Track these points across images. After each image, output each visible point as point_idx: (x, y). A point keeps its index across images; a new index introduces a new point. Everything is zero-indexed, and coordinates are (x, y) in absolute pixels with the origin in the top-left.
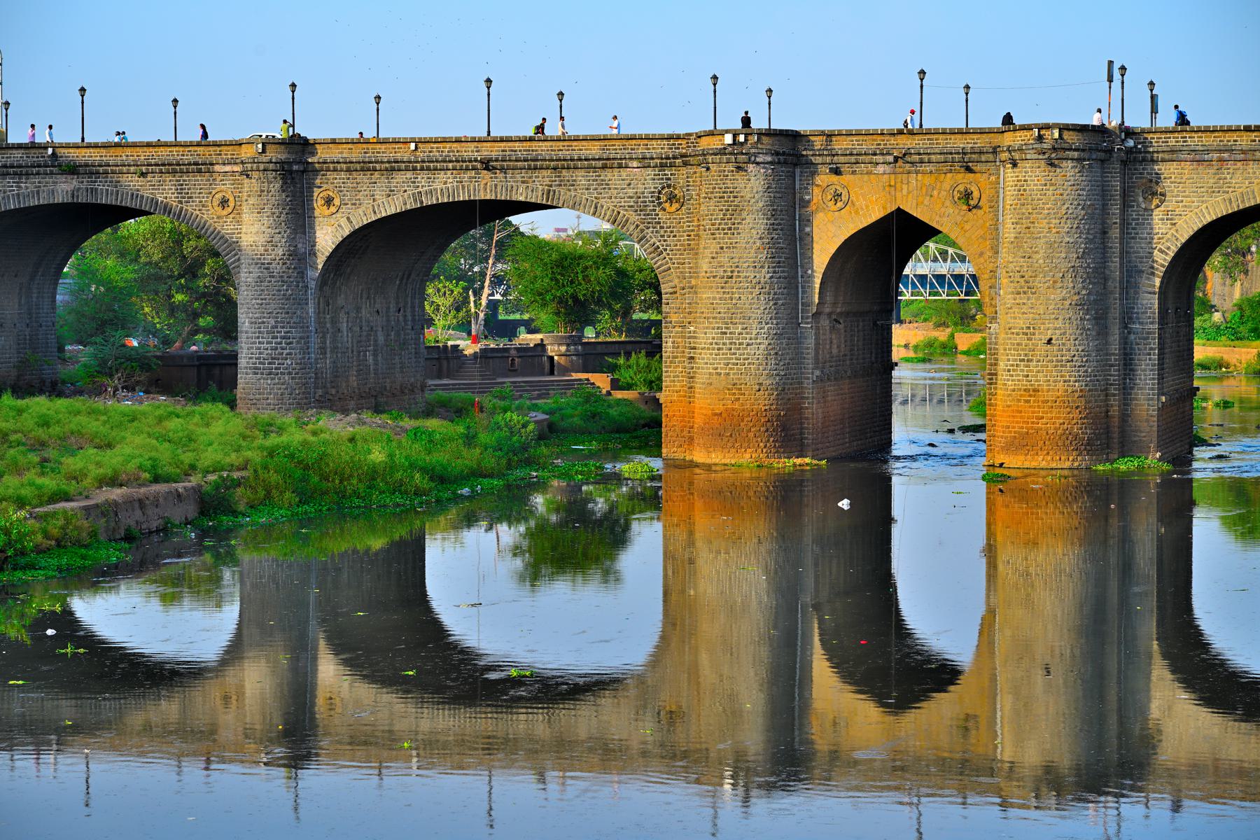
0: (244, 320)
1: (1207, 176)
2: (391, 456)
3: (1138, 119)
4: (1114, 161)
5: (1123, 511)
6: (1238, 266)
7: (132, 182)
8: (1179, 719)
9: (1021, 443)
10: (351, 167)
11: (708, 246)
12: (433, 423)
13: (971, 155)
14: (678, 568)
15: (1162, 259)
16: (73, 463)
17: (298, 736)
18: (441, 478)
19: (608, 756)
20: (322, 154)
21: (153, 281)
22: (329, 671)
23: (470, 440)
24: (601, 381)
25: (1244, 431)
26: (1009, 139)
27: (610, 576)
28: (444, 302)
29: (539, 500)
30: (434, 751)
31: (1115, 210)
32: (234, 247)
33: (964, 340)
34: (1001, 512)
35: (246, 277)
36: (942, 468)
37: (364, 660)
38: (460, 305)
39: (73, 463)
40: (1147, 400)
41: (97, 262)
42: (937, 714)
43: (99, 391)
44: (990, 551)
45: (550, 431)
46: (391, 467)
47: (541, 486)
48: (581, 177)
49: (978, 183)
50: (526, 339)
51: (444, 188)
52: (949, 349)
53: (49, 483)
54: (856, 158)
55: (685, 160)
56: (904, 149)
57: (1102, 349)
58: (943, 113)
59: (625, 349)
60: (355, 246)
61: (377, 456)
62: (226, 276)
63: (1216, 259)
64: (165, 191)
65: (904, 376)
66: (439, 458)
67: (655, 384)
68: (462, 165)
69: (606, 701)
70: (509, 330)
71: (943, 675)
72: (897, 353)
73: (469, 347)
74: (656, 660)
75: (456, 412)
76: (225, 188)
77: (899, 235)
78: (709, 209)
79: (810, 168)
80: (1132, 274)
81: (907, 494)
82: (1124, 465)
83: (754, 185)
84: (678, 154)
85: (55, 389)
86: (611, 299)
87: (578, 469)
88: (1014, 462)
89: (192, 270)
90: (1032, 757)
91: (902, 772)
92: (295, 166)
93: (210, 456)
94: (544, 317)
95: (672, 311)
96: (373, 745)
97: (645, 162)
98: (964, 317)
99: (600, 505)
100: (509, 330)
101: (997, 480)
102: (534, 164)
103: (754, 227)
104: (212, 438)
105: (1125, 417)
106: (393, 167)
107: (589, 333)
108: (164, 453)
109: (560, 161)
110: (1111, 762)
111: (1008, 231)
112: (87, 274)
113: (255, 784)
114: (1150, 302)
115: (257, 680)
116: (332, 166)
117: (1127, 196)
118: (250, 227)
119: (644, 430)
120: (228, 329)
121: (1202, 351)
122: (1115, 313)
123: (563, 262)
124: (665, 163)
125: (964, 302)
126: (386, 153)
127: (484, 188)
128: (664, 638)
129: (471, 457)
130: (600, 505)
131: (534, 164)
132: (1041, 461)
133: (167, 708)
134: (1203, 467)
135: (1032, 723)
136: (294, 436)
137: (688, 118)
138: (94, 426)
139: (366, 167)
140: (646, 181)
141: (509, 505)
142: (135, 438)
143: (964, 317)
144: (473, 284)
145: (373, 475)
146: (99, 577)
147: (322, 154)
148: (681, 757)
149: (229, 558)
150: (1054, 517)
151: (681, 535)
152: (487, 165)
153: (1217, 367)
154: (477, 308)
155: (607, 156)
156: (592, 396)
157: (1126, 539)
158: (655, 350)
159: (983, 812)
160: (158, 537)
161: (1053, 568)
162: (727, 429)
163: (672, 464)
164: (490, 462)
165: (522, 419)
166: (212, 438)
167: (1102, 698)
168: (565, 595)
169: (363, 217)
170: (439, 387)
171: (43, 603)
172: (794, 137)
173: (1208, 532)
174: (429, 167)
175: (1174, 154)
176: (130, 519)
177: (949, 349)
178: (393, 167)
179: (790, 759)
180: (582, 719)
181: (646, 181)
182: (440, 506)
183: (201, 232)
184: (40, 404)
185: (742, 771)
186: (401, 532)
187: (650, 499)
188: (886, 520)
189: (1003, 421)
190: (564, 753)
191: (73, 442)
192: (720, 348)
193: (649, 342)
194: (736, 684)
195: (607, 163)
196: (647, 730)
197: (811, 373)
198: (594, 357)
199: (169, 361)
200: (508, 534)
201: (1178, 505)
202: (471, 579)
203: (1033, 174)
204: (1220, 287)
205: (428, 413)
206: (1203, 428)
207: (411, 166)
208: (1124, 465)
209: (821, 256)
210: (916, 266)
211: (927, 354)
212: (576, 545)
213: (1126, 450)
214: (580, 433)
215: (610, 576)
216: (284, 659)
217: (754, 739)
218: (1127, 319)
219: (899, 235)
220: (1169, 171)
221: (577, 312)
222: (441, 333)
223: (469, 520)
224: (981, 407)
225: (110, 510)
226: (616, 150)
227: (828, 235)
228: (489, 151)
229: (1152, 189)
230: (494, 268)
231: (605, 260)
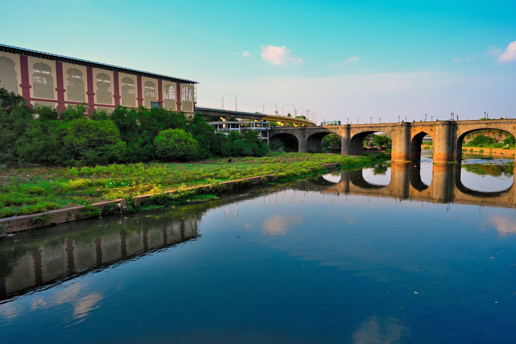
0: (342, 145)
1: (465, 127)
2: (164, 180)
3: (456, 120)
4: (452, 126)
5: (451, 168)
6: (469, 137)
7: (330, 130)
8: (458, 194)
9: (438, 160)
10: (355, 128)
11: (398, 136)
12: (364, 157)
13: (432, 125)
14: (393, 174)
15: (458, 137)
16: (323, 161)
17: (347, 191)
18: (364, 163)
19: (384, 195)
20: (352, 126)
21: (332, 140)
22: (351, 184)
23: (368, 159)
24: (384, 152)
25: (469, 158)
26: (437, 123)
27: (384, 174)
28: (365, 143)
29: (376, 166)
30: (362, 193)
31: (452, 131)
32: (341, 137)
33: (431, 147)
34: (435, 168)
35: (342, 140)
36: (427, 162)
37: (355, 183)
38: (367, 143)
39: (323, 161)
40: (455, 154)
41: (326, 138)
42: (425, 192)
43: (326, 153)
44: (433, 172)
45: (378, 157)
46: (359, 162)
47: (376, 164)
48: (382, 128)
49: (433, 128)
50: (375, 147)
51: (366, 130)
52: (429, 148)
53: (320, 163)
54: (417, 125)
55: (395, 126)
56: (423, 124)
57: (449, 148)
58: (429, 120)
59: (387, 148)
60: (355, 137)
61: (357, 160)
62: (340, 140)
63: (466, 136)
64: (334, 131)
65: (423, 151)
66: (364, 160)
67: (391, 152)
68: (368, 127)
69: (384, 188)
70: (373, 145)
71: (425, 187)
72: (422, 148)
73: (368, 148)
74: (390, 184)
75: (366, 155)
76: (340, 130)
77: (423, 134)
78: (398, 132)
79: (411, 127)
80: (454, 139)
81: (422, 165)
82: (452, 162)
83: (404, 129)
84: (394, 126)
85: (321, 153)
86: (385, 143)
87: (380, 159)
88: (436, 162)
89: (336, 139)
90: (438, 197)
91: (421, 198)
92: (348, 128)
93: (338, 160)
94: (377, 144)
95: (393, 144)
96: (356, 192)
97: (390, 126)
98: (431, 144)
99: (384, 166)
100: (373, 145)
101: (434, 164)
102: (376, 127)
103: (403, 134)
104: (338, 158)
105: (452, 157)
106: (360, 128)
107: (383, 146)
108: (333, 160)
109: (380, 127)
110: (448, 198)
111: (437, 134)
112: (325, 140)
113: (343, 196)
114: (456, 142)
115: (343, 185)
116: (353, 128)
117: (453, 130)
118: (343, 134)
119: (389, 158)
120: (340, 146)
121: (463, 148)
122: (451, 144)
123: (380, 138)
124: (393, 126)
125: (431, 142)
126: (359, 126)
127: (370, 130)
128: (391, 182)
129: (368, 160)
130: (384, 166)
131: (376, 127)
132: (440, 162)
133: (333, 187)
134: (463, 163)
135: (437, 192)
136: (348, 158)
137: (396, 121)
138: (325, 157)
139: (356, 128)
140: (390, 129)
141: (372, 166)
142: (329, 158)
143: (431, 144)
144: (369, 140)
145: (356, 162)
146: (325, 173)
147: (352, 126)
148: (392, 195)
149: (340, 172)
150: (441, 168)
151: (393, 170)
152: (371, 127)
153: (465, 150)
154: (369, 143)
155: (385, 126)
156: (383, 153)
157: (451, 171)
158: (391, 148)
159: (431, 203)
160: (333, 169)
161: (441, 175)
162: (400, 158)
163: (392, 162)
164: (370, 161)
165: (374, 156)
166: (338, 158)
167: (467, 201)
168: (379, 176)
169: (356, 133)
170: (364, 152)
171: (319, 176)
172: (409, 123)
173: (463, 171)
174: (364, 127)
175: (460, 124)
176: (329, 167)
177: (429, 148)
178: (360, 128)
179: (406, 196)
180: (380, 190)
181: (390, 129)
182: (364, 166)
183: (337, 135)
184: (319, 154)
185: (400, 197)
186: (360, 169)
187: (390, 165)
188: (420, 168)
189: (435, 157)
190: (378, 194)
191: (323, 158)
192: (398, 149)
193: (390, 147)
194: (399, 186)
195: (385, 127)
196: (389, 192)
197: (410, 151)
198: (383, 149)
199: (334, 149)
200: (372, 169)
201: (459, 167)
202: (368, 174)
203: (441, 127)
204: (466, 140)
205: (363, 155)
206: (463, 158)
207: (362, 127)
208: (452, 162)
209: (412, 137)
210: (425, 138)
211: (426, 148)
212: (381, 170)
213: (452, 160)
214: (382, 158)
215: (384, 174)
216: (346, 182)
217: (401, 193)
218: (453, 144)
219: (423, 134)
220: (459, 126)
221: (381, 144)
222: (365, 146)
223: (368, 168)
224: (432, 155)
225: (327, 166)
226: (387, 125)
227: (413, 135)
228: (372, 125)
229: (457, 128)
230: (371, 138)
231: (385, 137)
